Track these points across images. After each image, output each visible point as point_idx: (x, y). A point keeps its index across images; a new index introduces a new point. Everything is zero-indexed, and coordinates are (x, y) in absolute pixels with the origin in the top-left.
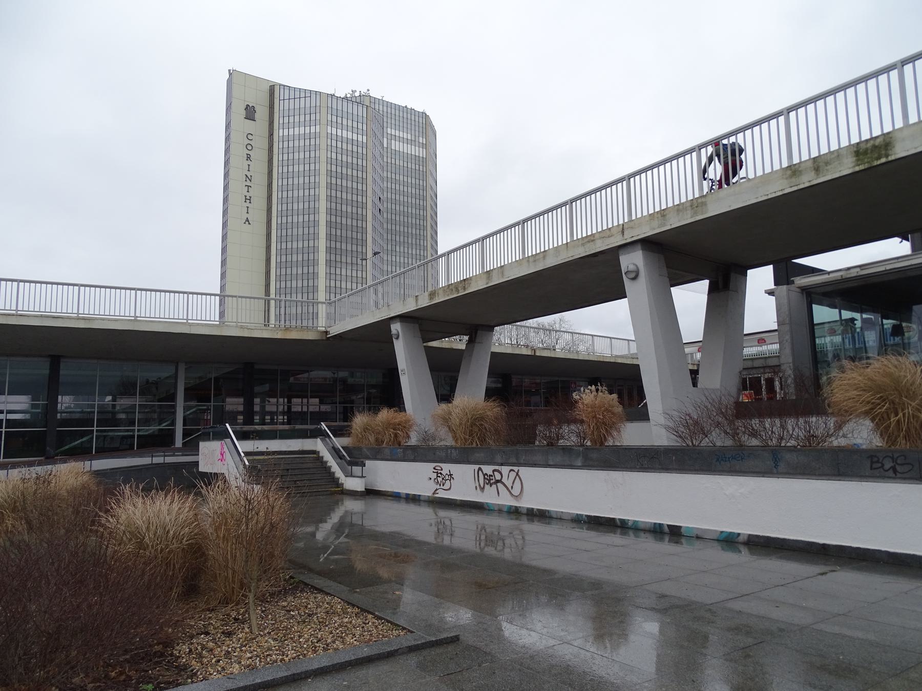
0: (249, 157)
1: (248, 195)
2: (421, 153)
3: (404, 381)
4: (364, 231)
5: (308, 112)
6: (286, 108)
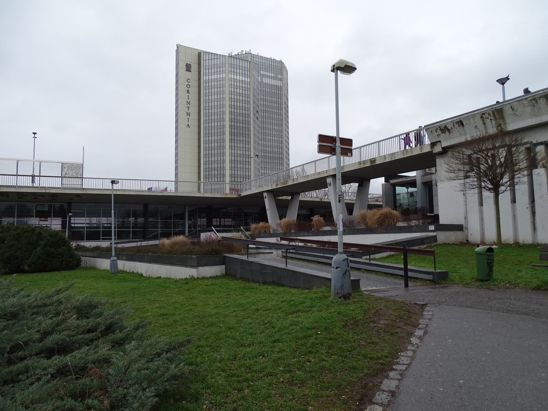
0: (188, 92)
1: (188, 112)
2: (279, 83)
3: (268, 213)
4: (249, 129)
5: (219, 66)
6: (207, 64)
